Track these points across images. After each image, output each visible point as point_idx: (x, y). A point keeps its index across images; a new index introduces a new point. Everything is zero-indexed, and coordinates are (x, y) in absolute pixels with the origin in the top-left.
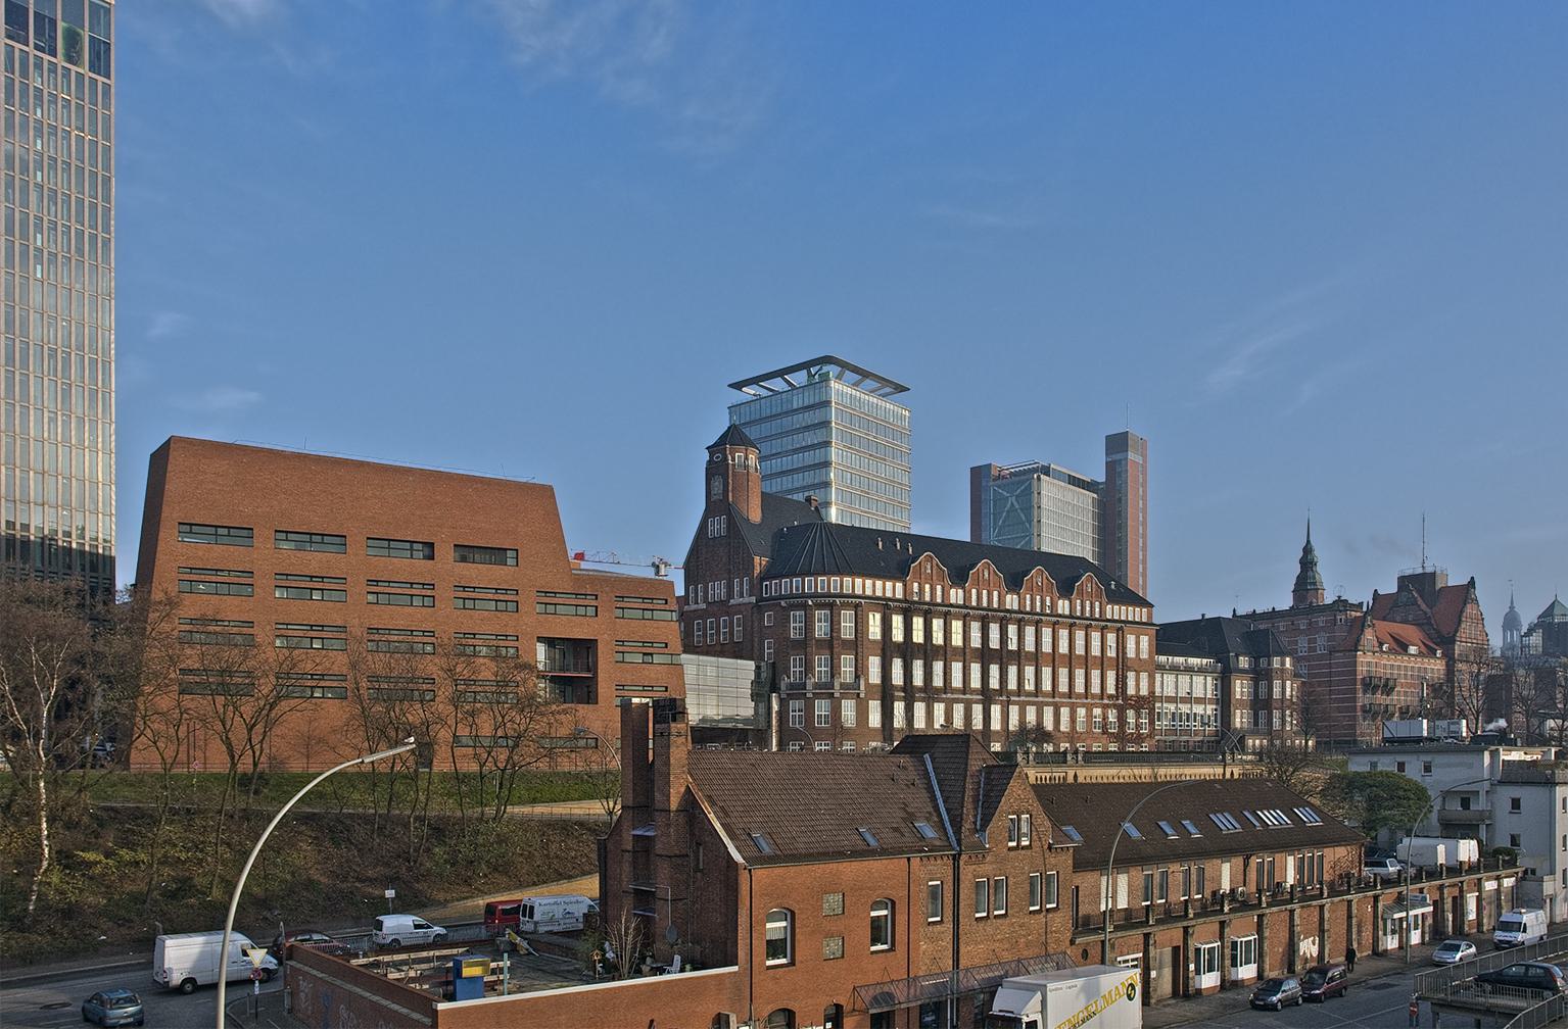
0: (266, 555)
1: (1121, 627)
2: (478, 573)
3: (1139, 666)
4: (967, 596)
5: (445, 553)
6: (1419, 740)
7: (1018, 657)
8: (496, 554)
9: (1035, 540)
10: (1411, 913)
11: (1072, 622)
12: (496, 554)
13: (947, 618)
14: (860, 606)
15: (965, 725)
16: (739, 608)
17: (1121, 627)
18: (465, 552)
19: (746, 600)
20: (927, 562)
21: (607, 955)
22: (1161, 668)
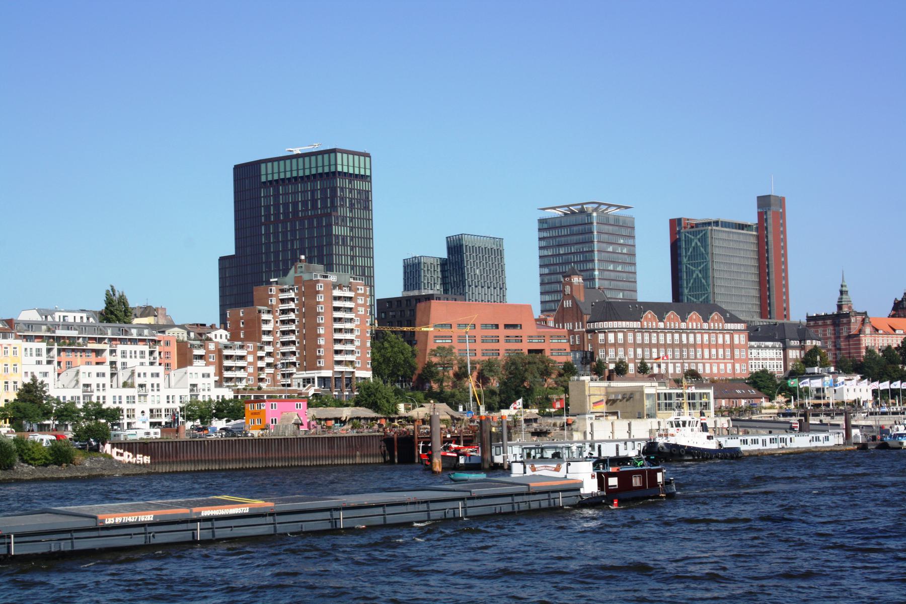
0: (502, 332)
1: (732, 332)
2: (512, 332)
3: (739, 346)
4: (688, 325)
5: (501, 327)
6: (814, 373)
7: (702, 346)
8: (514, 326)
9: (711, 298)
10: (780, 436)
11: (664, 331)
12: (514, 326)
13: (688, 334)
14: (615, 331)
15: (264, 331)
16: (578, 333)
17: (732, 332)
18: (507, 326)
19: (581, 329)
20: (649, 314)
21: (224, 341)
22: (752, 347)
